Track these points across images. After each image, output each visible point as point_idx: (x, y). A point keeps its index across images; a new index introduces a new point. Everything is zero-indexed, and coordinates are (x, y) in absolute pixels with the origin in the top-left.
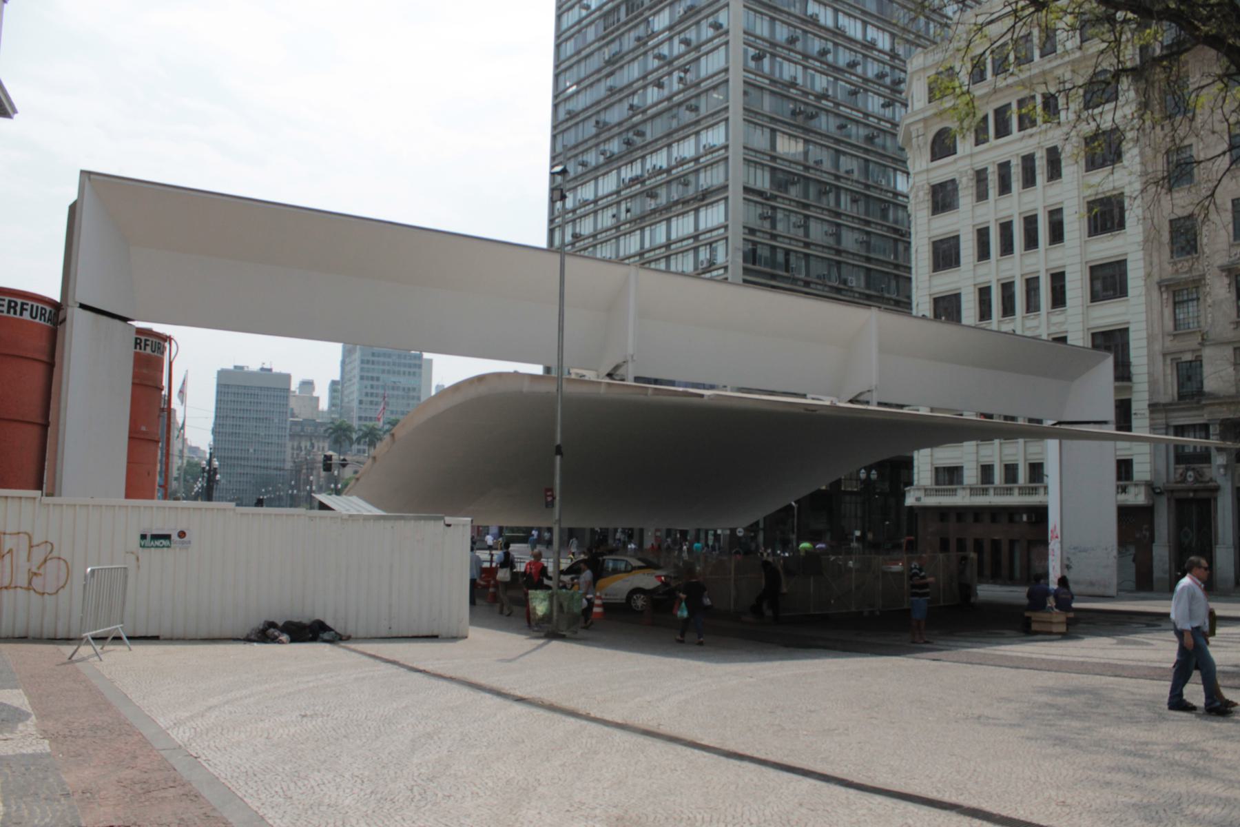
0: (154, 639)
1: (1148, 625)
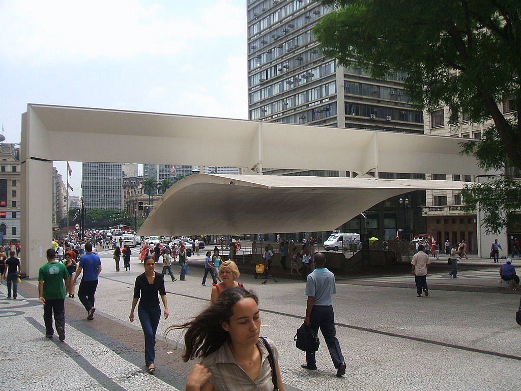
0: (46, 161)
1: (276, 281)
